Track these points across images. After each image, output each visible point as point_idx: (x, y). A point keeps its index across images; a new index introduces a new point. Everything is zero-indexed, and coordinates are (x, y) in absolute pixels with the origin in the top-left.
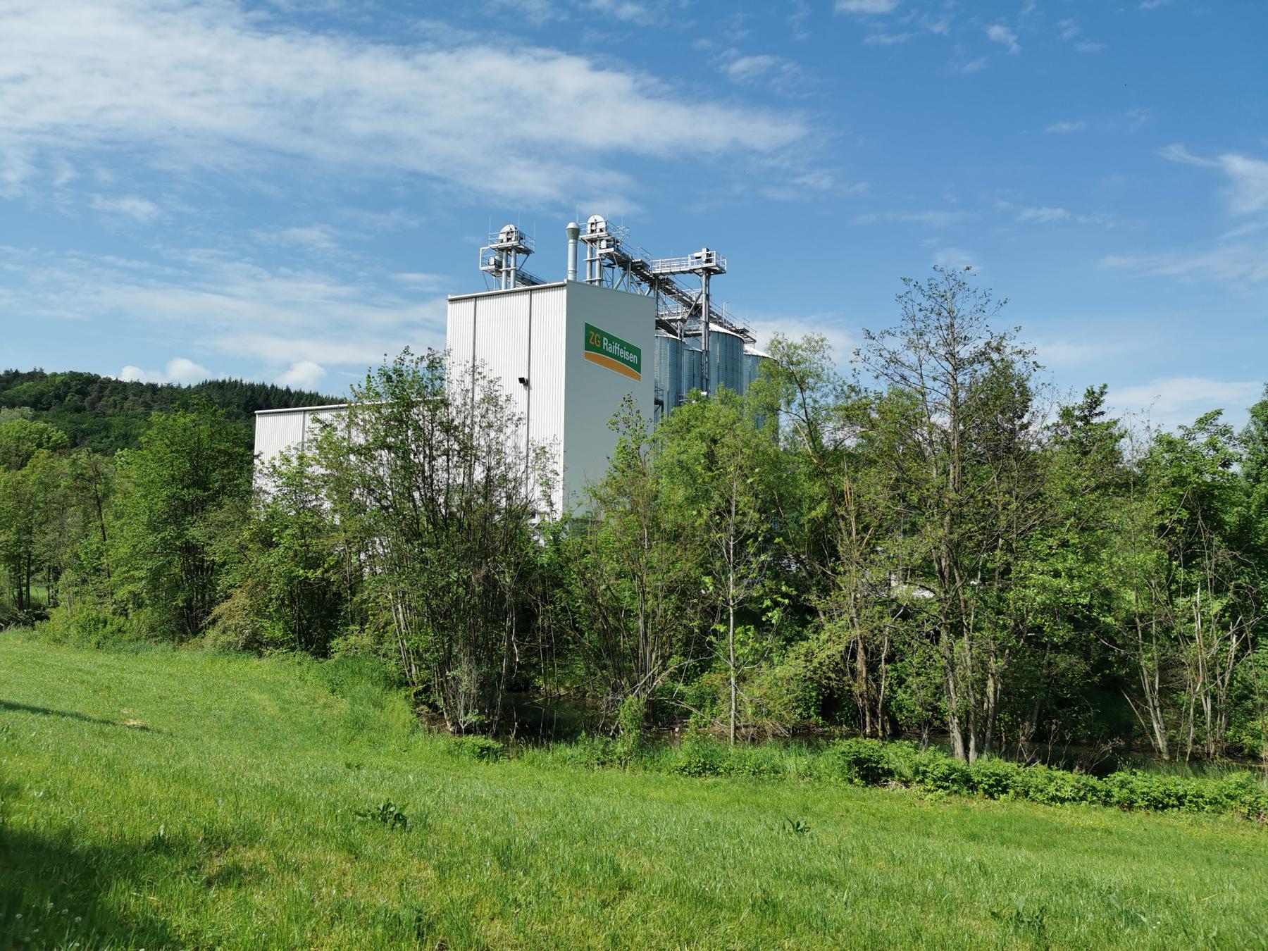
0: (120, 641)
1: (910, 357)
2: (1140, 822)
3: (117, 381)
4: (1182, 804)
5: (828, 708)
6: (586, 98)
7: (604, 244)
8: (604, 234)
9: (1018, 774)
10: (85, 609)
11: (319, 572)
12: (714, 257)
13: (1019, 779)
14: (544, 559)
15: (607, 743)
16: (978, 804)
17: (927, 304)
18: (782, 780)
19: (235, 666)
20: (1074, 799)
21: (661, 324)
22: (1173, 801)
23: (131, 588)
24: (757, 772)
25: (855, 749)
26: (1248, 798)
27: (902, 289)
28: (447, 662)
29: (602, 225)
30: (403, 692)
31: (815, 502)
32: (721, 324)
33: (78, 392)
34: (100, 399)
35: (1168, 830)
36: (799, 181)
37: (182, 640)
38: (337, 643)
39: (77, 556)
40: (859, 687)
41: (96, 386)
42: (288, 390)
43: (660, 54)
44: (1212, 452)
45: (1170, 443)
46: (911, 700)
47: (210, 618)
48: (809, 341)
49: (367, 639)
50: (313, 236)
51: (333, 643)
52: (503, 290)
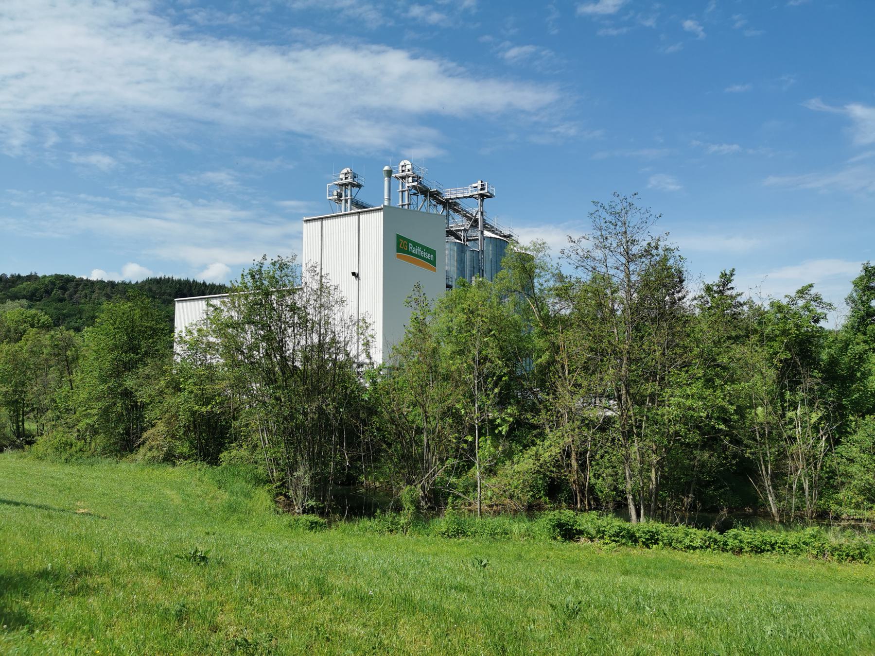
0: (81, 457)
1: (598, 254)
2: (744, 561)
3: (87, 280)
4: (774, 549)
5: (554, 488)
6: (407, 78)
7: (410, 179)
8: (410, 173)
9: (666, 531)
10: (59, 436)
11: (209, 407)
12: (486, 187)
13: (665, 534)
14: (366, 397)
15: (394, 518)
16: (637, 552)
17: (609, 218)
18: (509, 539)
19: (157, 473)
20: (702, 547)
21: (450, 233)
22: (768, 547)
23: (88, 421)
24: (493, 534)
25: (557, 516)
26: (816, 544)
27: (593, 209)
28: (293, 467)
29: (409, 167)
30: (267, 488)
31: (540, 352)
32: (493, 232)
33: (60, 288)
34: (76, 292)
35: (761, 566)
36: (554, 130)
37: (122, 456)
38: (224, 455)
39: (54, 401)
40: (573, 477)
41: (73, 284)
42: (204, 283)
43: (458, 47)
44: (807, 313)
45: (779, 307)
46: (603, 486)
47: (141, 440)
48: (535, 244)
49: (244, 453)
50: (222, 177)
51: (221, 455)
52: (343, 213)
